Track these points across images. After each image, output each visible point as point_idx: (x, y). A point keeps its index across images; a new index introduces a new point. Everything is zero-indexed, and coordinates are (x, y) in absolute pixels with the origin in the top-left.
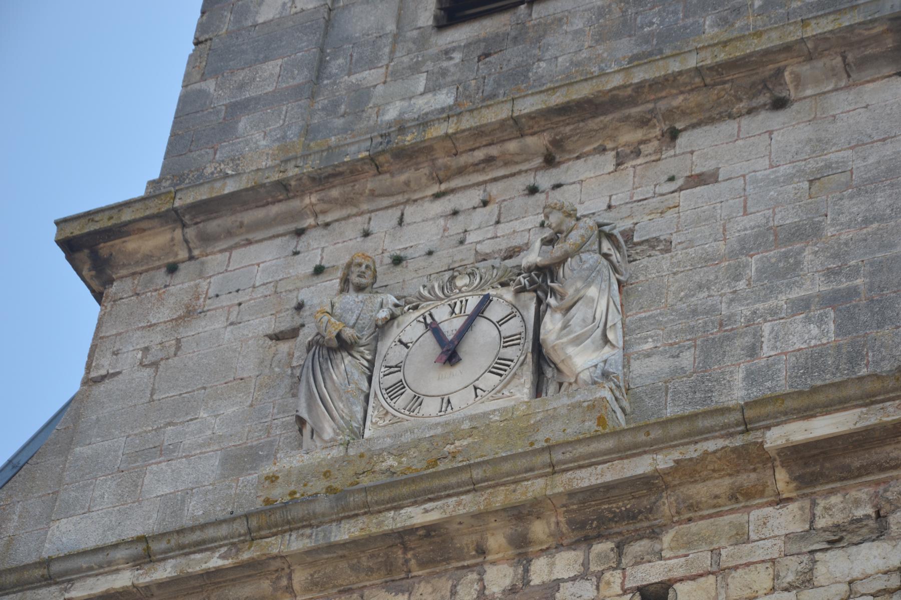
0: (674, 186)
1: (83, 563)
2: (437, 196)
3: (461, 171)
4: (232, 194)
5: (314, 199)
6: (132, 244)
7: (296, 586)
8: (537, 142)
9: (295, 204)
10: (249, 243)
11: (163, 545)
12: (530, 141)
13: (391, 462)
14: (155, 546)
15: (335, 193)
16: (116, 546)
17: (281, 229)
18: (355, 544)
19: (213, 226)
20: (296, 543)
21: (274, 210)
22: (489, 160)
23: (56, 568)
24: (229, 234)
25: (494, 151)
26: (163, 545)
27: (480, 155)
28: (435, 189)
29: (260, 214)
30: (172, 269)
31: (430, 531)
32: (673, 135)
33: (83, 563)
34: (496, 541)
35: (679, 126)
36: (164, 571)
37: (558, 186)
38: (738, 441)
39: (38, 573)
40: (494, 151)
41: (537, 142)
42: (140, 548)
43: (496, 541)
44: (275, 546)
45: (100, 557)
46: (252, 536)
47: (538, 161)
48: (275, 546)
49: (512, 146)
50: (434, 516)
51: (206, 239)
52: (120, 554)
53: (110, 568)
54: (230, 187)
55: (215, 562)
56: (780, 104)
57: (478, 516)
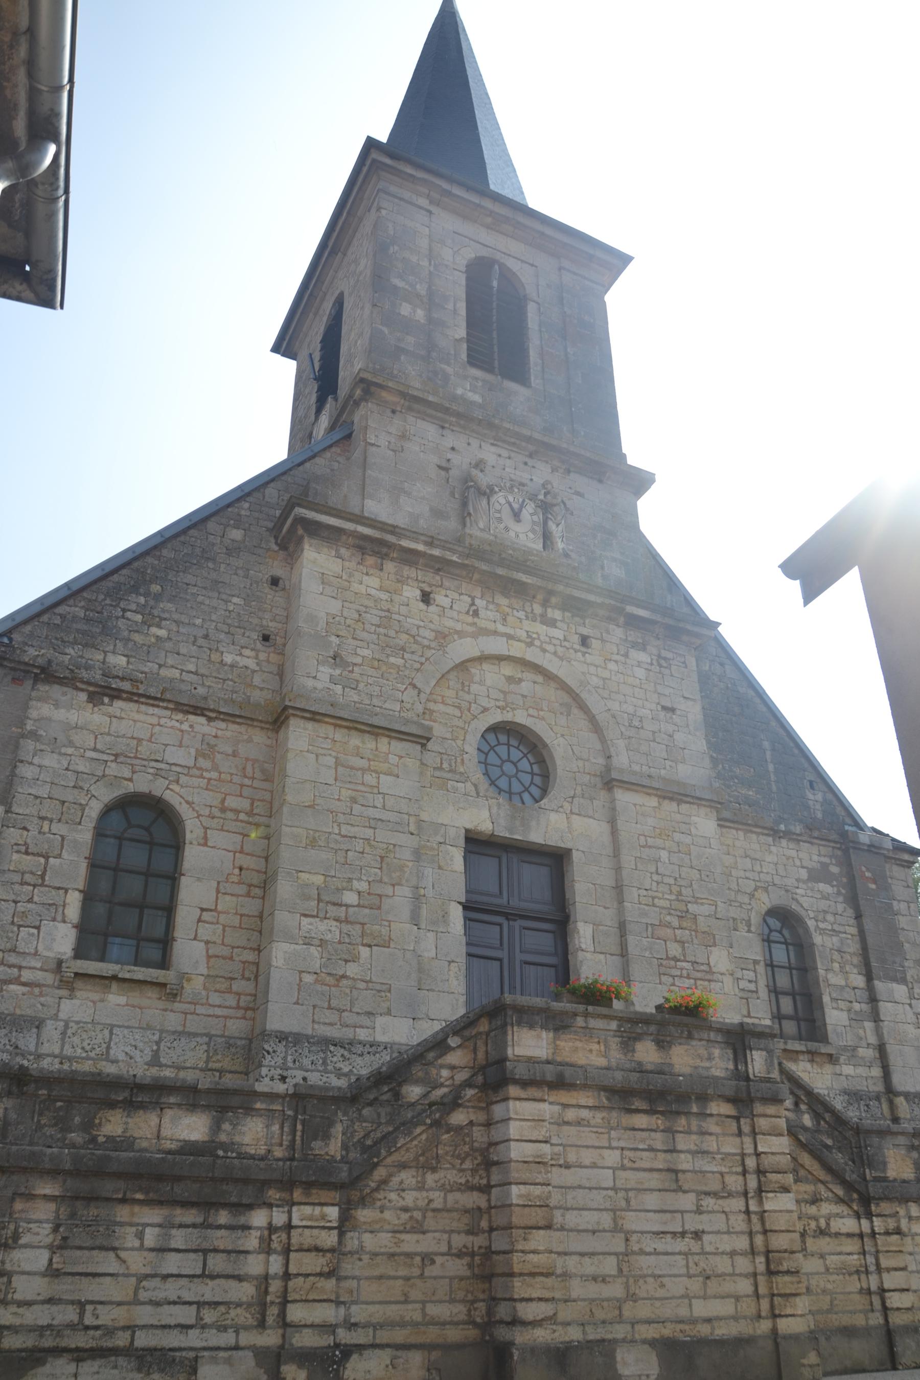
0: (569, 490)
1: (408, 534)
2: (492, 444)
3: (504, 441)
4: (431, 402)
5: (454, 420)
6: (384, 394)
7: (474, 578)
8: (531, 448)
9: (447, 417)
10: (424, 419)
11: (438, 543)
12: (530, 446)
13: (511, 552)
14: (436, 542)
15: (462, 422)
16: (422, 534)
17: (437, 422)
18: (501, 576)
19: (416, 406)
20: (484, 567)
21: (439, 415)
22: (514, 444)
23: (397, 530)
24: (419, 412)
25: (518, 442)
26: (438, 543)
27: (513, 440)
28: (492, 441)
29: (434, 413)
30: (394, 412)
31: (523, 584)
32: (569, 472)
33: (408, 534)
34: (540, 597)
35: (572, 469)
36: (436, 552)
37: (534, 467)
38: (619, 605)
39: (390, 528)
40: (518, 442)
41: (531, 448)
42: (430, 540)
43: (540, 597)
44: (477, 564)
45: (415, 535)
46: (468, 556)
47: (527, 453)
48: (477, 564)
49: (524, 444)
50: (529, 581)
51: (410, 409)
52: (423, 538)
53: (416, 540)
54: (431, 398)
55: (455, 558)
56: (600, 481)
57: (540, 587)
